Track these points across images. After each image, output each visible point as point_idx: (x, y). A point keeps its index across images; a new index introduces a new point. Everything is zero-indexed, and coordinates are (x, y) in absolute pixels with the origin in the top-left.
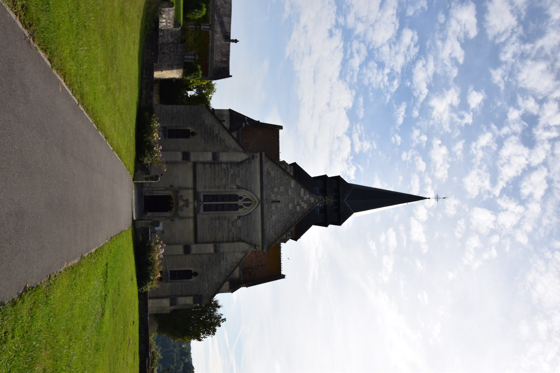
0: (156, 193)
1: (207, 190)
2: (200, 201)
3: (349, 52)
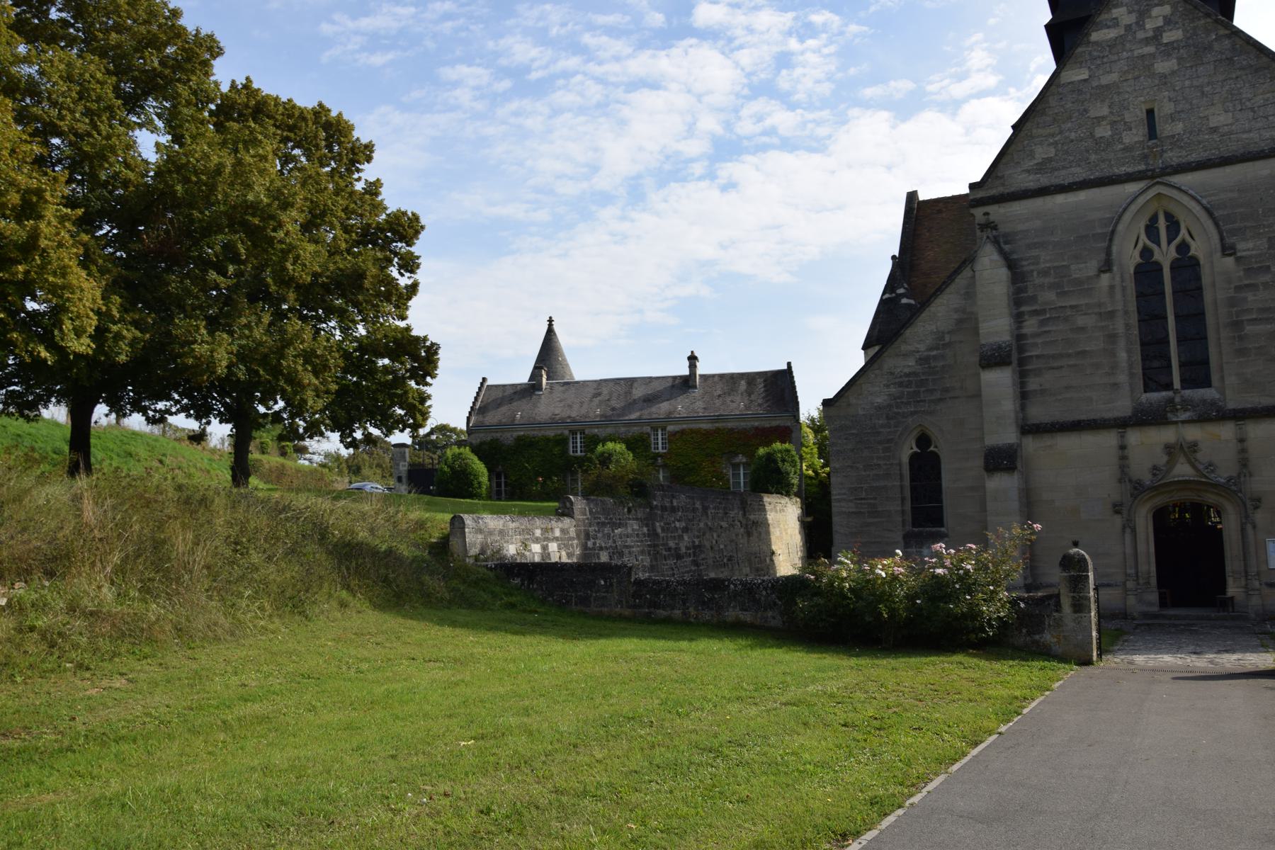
0: (1148, 565)
1: (1122, 378)
2: (1171, 401)
3: (765, 139)
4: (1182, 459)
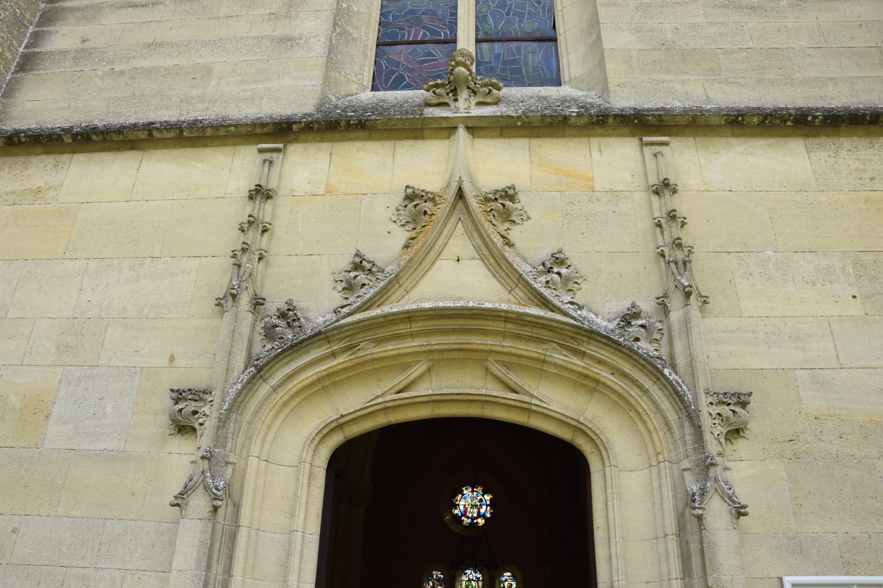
4: (459, 243)
